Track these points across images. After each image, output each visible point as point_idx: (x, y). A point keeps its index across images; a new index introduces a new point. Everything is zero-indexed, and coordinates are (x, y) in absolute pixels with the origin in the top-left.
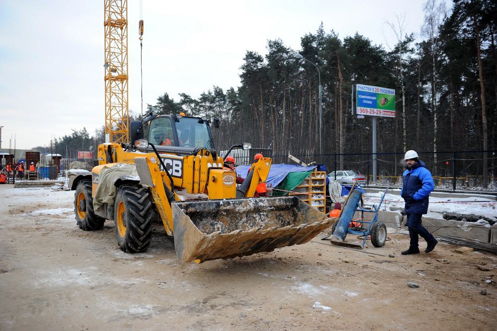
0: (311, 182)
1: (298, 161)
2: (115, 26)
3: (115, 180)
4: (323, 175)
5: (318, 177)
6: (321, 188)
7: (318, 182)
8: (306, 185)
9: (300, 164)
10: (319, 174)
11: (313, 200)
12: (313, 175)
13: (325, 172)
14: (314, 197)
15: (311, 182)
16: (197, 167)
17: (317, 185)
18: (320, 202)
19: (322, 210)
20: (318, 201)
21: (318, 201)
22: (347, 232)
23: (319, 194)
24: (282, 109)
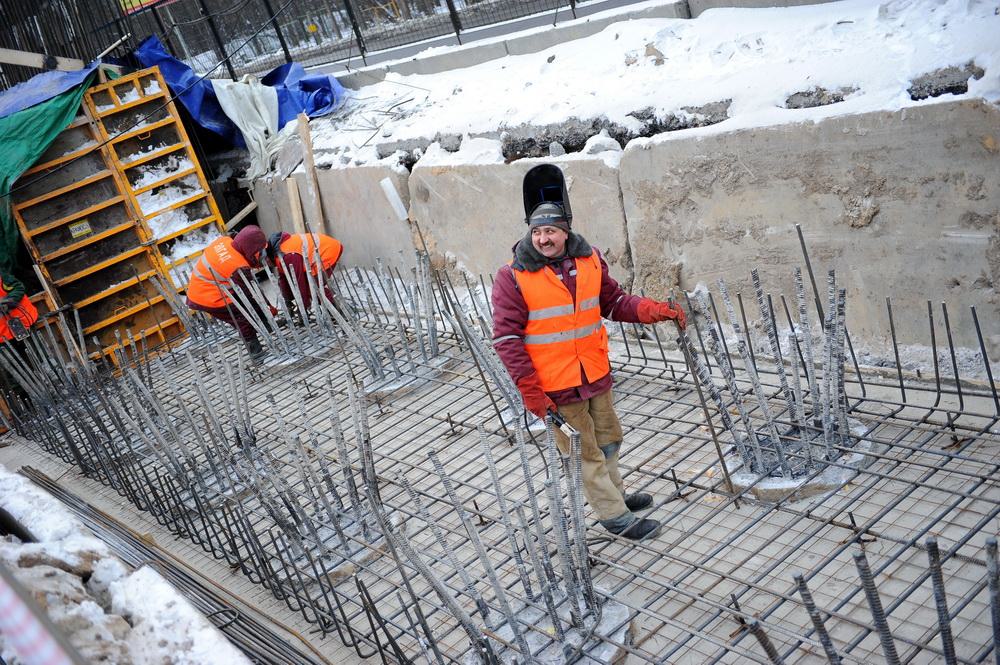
0: (100, 132)
1: (34, 60)
2: (122, 425)
3: (982, 79)
4: (154, 84)
5: (133, 98)
6: (166, 134)
7: (140, 117)
8: (87, 147)
9: (50, 65)
10: (130, 84)
11: (142, 191)
12: (103, 97)
13: (155, 69)
14: (147, 175)
15: (100, 132)
16: (938, 315)
17: (142, 127)
18: (183, 186)
19: (205, 210)
20: (174, 183)
21: (174, 183)
22: (859, 439)
23: (163, 159)
24: (298, 97)
